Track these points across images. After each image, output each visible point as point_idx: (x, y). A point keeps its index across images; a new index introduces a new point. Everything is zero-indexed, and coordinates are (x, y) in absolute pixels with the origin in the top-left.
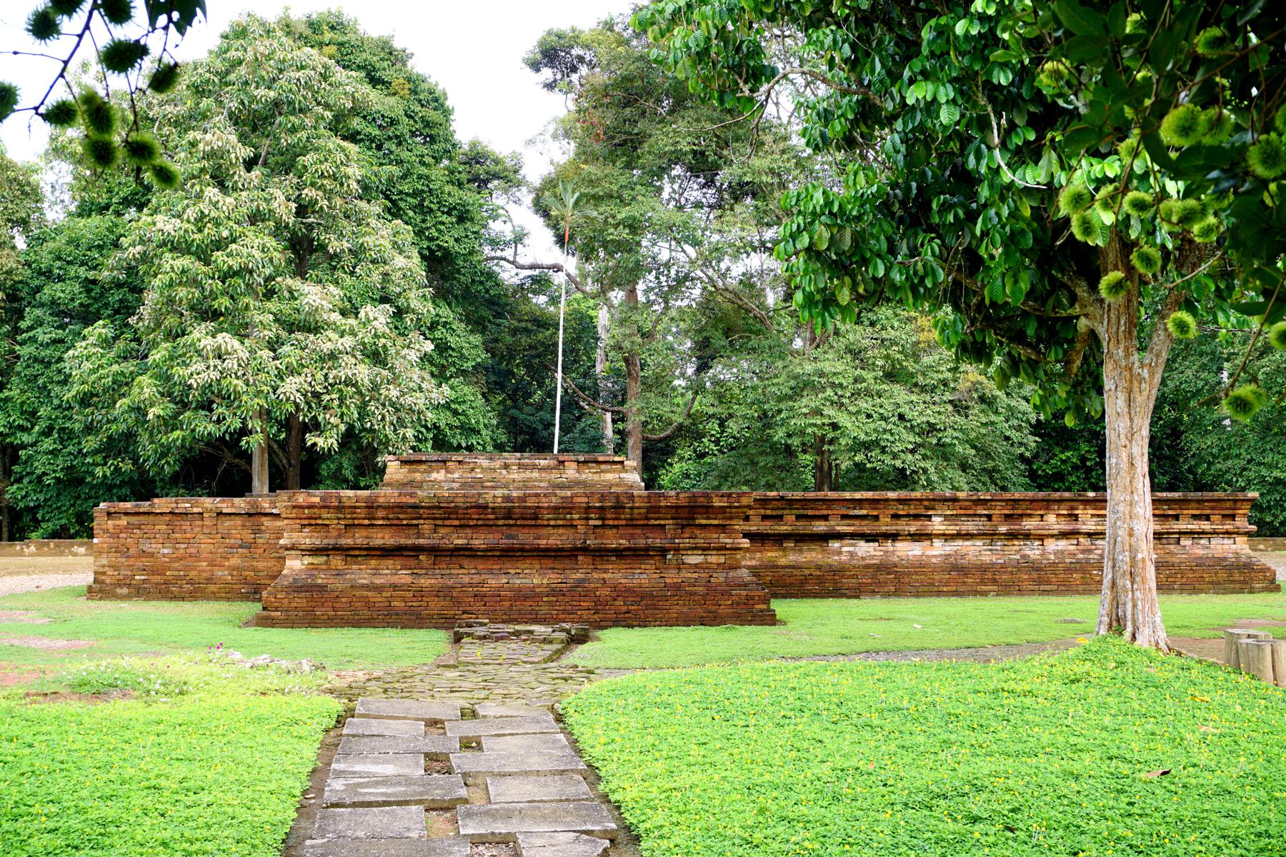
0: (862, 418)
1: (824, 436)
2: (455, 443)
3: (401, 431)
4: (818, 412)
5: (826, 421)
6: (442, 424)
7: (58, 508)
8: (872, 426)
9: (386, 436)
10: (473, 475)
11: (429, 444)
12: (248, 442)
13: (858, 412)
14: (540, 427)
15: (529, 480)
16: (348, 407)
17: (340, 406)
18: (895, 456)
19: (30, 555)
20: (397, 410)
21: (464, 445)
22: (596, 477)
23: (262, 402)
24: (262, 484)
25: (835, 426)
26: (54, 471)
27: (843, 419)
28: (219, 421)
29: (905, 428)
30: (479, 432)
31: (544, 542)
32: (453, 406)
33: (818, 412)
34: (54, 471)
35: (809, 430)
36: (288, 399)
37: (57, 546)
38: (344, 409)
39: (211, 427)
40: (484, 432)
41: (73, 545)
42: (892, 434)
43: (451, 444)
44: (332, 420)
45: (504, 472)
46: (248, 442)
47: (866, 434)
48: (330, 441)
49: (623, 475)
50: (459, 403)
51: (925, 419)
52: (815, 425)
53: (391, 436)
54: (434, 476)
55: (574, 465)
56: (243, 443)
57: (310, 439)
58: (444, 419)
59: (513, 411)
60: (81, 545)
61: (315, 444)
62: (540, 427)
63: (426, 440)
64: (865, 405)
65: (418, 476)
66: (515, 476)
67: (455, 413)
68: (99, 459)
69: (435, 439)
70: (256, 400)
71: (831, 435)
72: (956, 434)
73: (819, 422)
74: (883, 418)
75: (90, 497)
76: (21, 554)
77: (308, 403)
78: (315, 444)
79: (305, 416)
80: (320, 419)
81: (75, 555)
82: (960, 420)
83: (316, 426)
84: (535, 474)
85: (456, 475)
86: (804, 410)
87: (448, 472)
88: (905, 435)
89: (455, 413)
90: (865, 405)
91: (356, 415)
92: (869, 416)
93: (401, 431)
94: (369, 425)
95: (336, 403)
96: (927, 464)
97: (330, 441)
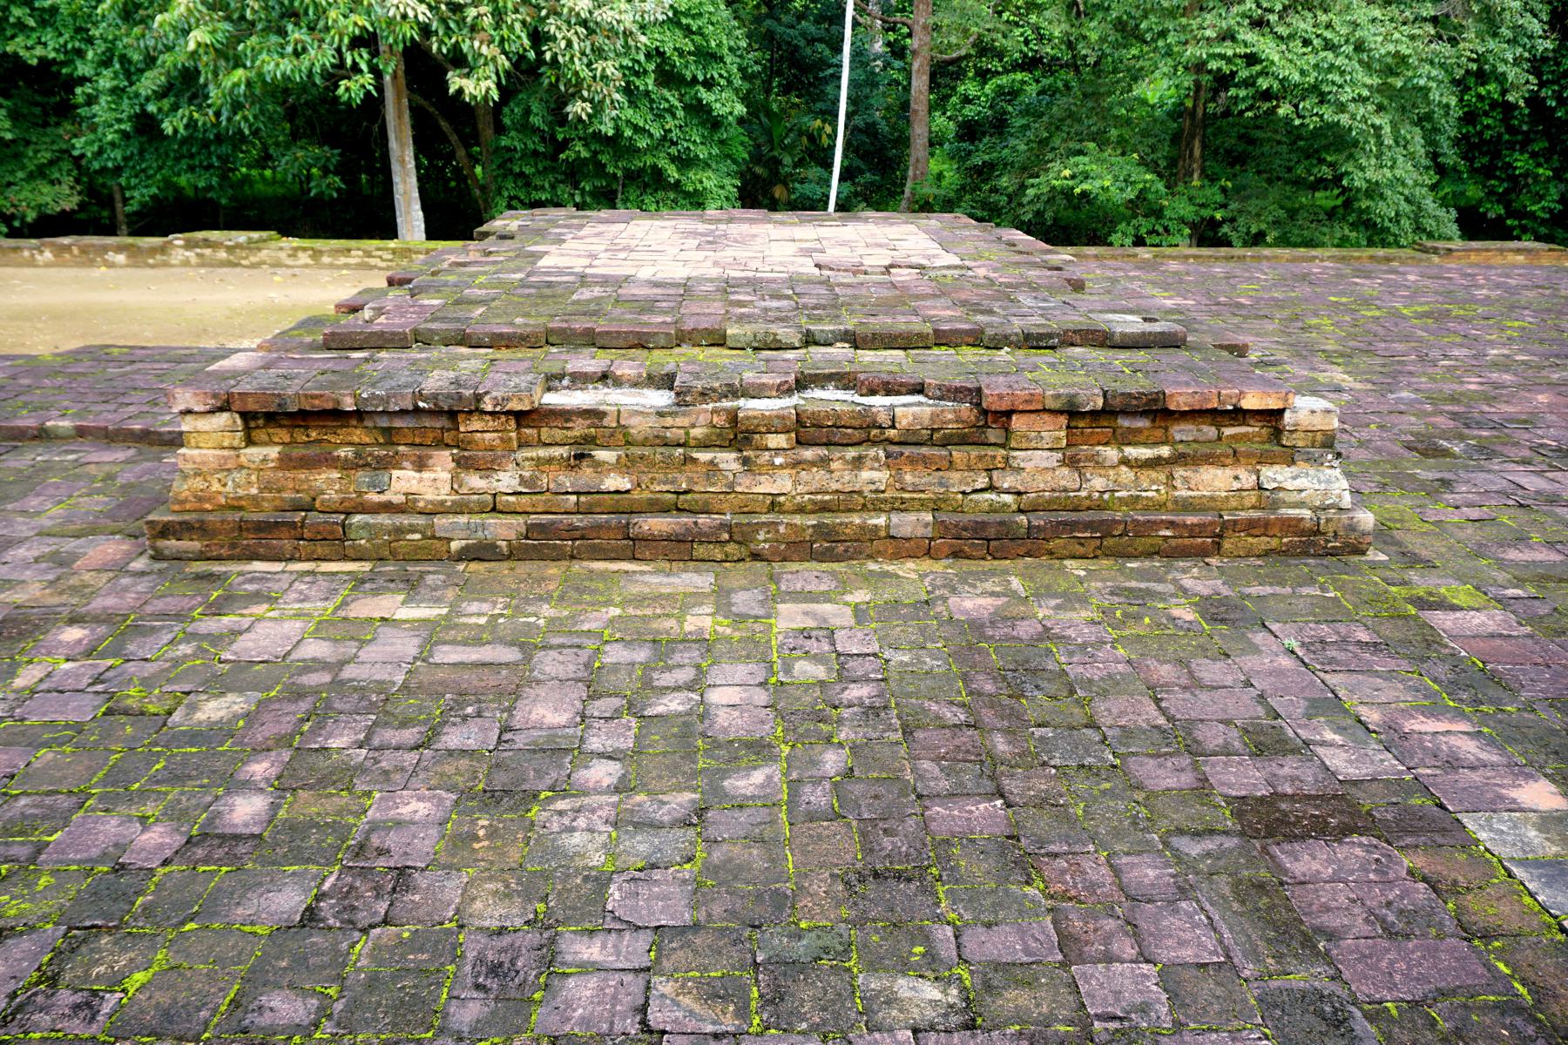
0: (1297, 45)
1: (1233, 74)
2: (689, 76)
3: (599, 66)
4: (1228, 36)
5: (1241, 50)
6: (668, 49)
7: (143, 171)
8: (1312, 60)
9: (576, 73)
10: (586, 477)
11: (650, 81)
12: (347, 89)
13: (1291, 37)
14: (802, 43)
15: (847, 501)
16: (511, 28)
17: (497, 27)
18: (1342, 108)
19: (48, 265)
20: (591, 32)
21: (701, 78)
22: (1152, 487)
23: (362, 21)
24: (402, 145)
25: (1252, 59)
26: (119, 121)
27: (1268, 48)
28: (297, 54)
29: (1360, 62)
30: (721, 59)
31: (856, 519)
32: (684, 21)
33: (1228, 36)
34: (119, 121)
35: (1213, 65)
36: (404, 16)
37: (84, 250)
38: (505, 32)
39: (286, 66)
40: (728, 60)
41: (105, 249)
42: (1342, 73)
43: (683, 76)
44: (484, 50)
45: (728, 460)
46: (347, 89)
47: (1303, 73)
48: (484, 84)
49: (1274, 475)
50: (693, 17)
51: (1391, 48)
52: (1222, 57)
53: (585, 73)
54: (404, 481)
55: (1054, 430)
56: (341, 91)
57: (455, 81)
58: (671, 42)
59: (768, 22)
60: (119, 249)
61: (460, 91)
62: (802, 43)
63: (645, 72)
64: (1302, 25)
65: (328, 483)
66: (781, 484)
67: (688, 31)
68: (166, 104)
69: (659, 70)
70: (353, 17)
71: (1244, 74)
72: (1434, 73)
73: (1230, 53)
74: (1329, 46)
75: (183, 157)
76: (32, 263)
77: (444, 21)
78: (460, 91)
79: (441, 42)
80: (465, 47)
81: (111, 265)
82: (1444, 49)
83: (458, 60)
84: (873, 477)
85: (506, 480)
86: (1209, 33)
87: (463, 464)
88: (1361, 76)
89: (688, 31)
90: (1302, 25)
91: (527, 43)
92: (1306, 43)
93: (599, 66)
94: (548, 56)
95: (487, 21)
96: (1380, 120)
97: (484, 84)
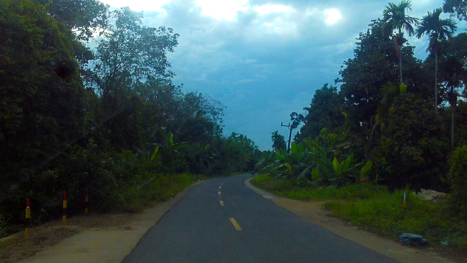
20: (148, 48)
